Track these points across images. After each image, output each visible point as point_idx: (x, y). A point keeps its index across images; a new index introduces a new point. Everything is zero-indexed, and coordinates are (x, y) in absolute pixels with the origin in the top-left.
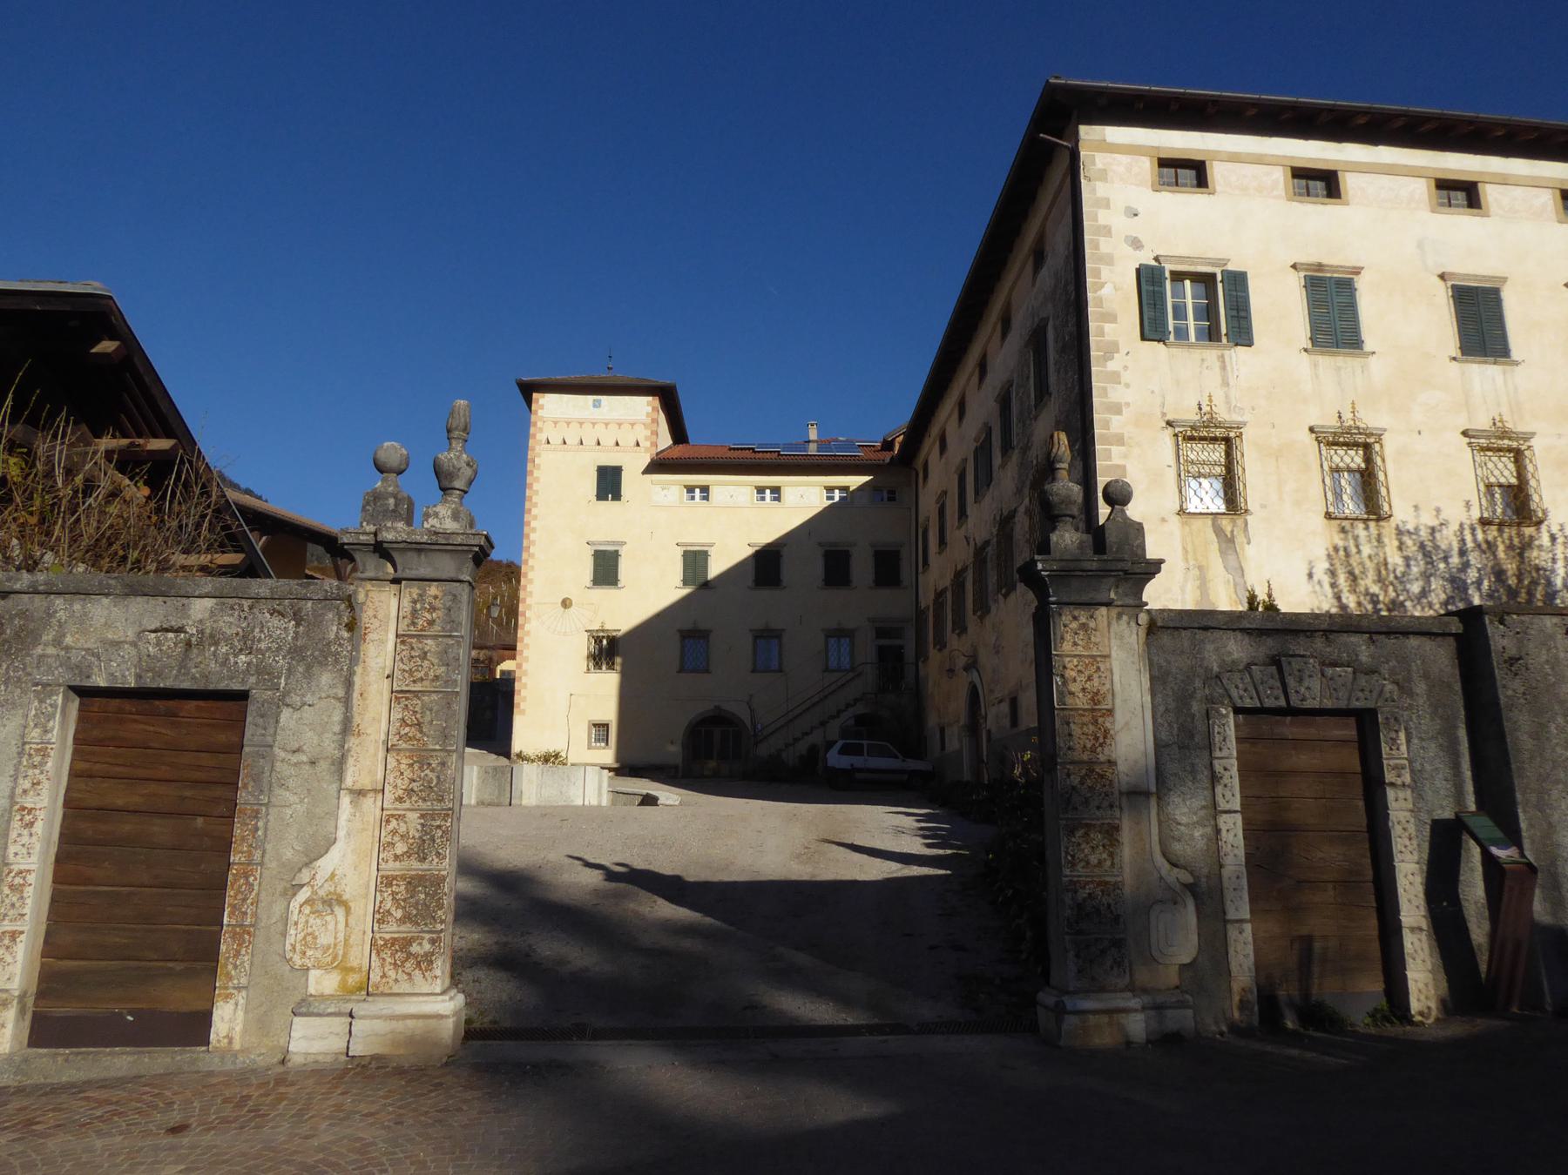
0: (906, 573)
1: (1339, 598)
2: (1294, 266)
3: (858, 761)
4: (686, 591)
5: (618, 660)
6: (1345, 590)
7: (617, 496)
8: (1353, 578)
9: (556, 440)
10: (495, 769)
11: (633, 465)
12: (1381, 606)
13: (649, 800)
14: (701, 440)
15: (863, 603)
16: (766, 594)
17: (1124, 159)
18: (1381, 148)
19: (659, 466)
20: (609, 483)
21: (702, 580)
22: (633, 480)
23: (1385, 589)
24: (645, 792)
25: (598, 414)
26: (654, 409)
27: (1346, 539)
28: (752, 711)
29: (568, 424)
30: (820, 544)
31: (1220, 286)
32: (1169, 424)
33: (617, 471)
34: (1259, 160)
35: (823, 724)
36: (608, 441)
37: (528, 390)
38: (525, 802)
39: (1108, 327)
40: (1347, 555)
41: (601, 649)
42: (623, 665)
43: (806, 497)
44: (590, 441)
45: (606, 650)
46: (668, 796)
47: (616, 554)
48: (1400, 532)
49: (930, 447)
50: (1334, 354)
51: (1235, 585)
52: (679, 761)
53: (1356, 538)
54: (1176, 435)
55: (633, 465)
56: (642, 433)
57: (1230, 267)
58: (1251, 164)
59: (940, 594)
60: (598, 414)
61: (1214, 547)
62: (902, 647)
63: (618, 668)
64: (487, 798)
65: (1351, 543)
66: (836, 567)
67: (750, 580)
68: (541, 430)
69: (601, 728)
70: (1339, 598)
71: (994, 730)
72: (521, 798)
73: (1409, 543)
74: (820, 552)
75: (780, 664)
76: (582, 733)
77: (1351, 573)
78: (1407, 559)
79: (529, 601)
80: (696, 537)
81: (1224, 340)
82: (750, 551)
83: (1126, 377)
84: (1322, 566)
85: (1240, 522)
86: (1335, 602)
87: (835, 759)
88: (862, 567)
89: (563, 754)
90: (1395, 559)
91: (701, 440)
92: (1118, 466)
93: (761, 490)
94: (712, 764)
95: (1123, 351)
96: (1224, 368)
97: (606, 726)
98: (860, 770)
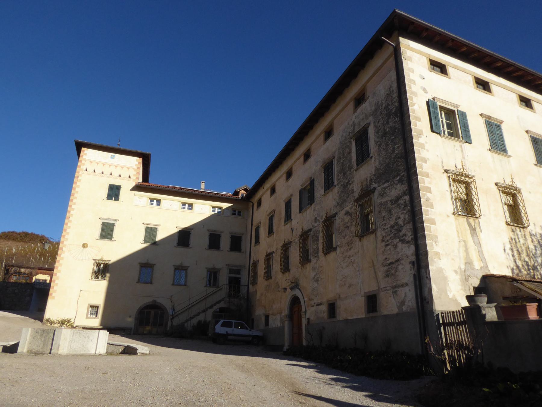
0: (245, 245)
1: (515, 262)
2: (481, 115)
3: (229, 330)
4: (146, 245)
5: (108, 275)
6: (517, 258)
7: (117, 199)
8: (519, 254)
9: (90, 170)
10: (43, 331)
11: (126, 186)
12: (530, 267)
13: (129, 351)
14: (152, 182)
15: (223, 259)
16: (182, 250)
17: (418, 56)
18: (501, 78)
19: (138, 188)
20: (114, 192)
21: (153, 241)
22: (125, 193)
23: (530, 259)
24: (126, 344)
25: (112, 161)
26: (139, 163)
27: (514, 235)
28: (172, 303)
29: (98, 163)
30: (208, 230)
31: (457, 116)
32: (446, 171)
33: (118, 188)
34: (464, 71)
35: (204, 311)
36: (116, 173)
37: (79, 146)
38: (60, 352)
39: (418, 123)
40: (516, 243)
41: (99, 269)
42: (110, 278)
43: (203, 210)
44: (107, 173)
45: (102, 270)
46: (142, 347)
47: (113, 225)
48: (531, 235)
49: (264, 193)
50: (499, 154)
51: (479, 251)
52: (132, 326)
53: (517, 235)
54: (449, 177)
55: (126, 186)
56: (132, 173)
57: (460, 109)
58: (462, 72)
59: (269, 256)
60: (112, 161)
61: (469, 232)
62: (240, 278)
63: (107, 279)
64: (35, 348)
65: (516, 237)
66: (214, 241)
67: (176, 242)
68: (84, 164)
69: (95, 308)
70: (515, 262)
71: (312, 318)
72: (58, 349)
73: (535, 240)
74: (209, 234)
75: (186, 282)
76: (84, 309)
77: (518, 251)
78: (535, 246)
79: (65, 243)
80: (152, 221)
81: (461, 138)
82: (177, 230)
83: (427, 146)
84: (508, 246)
85: (477, 221)
86: (514, 263)
87: (219, 329)
88: (225, 242)
89: (72, 321)
90: (532, 247)
91: (152, 182)
92: (428, 187)
93: (184, 204)
94: (148, 328)
95: (425, 135)
96: (462, 151)
97: (97, 307)
98: (231, 335)
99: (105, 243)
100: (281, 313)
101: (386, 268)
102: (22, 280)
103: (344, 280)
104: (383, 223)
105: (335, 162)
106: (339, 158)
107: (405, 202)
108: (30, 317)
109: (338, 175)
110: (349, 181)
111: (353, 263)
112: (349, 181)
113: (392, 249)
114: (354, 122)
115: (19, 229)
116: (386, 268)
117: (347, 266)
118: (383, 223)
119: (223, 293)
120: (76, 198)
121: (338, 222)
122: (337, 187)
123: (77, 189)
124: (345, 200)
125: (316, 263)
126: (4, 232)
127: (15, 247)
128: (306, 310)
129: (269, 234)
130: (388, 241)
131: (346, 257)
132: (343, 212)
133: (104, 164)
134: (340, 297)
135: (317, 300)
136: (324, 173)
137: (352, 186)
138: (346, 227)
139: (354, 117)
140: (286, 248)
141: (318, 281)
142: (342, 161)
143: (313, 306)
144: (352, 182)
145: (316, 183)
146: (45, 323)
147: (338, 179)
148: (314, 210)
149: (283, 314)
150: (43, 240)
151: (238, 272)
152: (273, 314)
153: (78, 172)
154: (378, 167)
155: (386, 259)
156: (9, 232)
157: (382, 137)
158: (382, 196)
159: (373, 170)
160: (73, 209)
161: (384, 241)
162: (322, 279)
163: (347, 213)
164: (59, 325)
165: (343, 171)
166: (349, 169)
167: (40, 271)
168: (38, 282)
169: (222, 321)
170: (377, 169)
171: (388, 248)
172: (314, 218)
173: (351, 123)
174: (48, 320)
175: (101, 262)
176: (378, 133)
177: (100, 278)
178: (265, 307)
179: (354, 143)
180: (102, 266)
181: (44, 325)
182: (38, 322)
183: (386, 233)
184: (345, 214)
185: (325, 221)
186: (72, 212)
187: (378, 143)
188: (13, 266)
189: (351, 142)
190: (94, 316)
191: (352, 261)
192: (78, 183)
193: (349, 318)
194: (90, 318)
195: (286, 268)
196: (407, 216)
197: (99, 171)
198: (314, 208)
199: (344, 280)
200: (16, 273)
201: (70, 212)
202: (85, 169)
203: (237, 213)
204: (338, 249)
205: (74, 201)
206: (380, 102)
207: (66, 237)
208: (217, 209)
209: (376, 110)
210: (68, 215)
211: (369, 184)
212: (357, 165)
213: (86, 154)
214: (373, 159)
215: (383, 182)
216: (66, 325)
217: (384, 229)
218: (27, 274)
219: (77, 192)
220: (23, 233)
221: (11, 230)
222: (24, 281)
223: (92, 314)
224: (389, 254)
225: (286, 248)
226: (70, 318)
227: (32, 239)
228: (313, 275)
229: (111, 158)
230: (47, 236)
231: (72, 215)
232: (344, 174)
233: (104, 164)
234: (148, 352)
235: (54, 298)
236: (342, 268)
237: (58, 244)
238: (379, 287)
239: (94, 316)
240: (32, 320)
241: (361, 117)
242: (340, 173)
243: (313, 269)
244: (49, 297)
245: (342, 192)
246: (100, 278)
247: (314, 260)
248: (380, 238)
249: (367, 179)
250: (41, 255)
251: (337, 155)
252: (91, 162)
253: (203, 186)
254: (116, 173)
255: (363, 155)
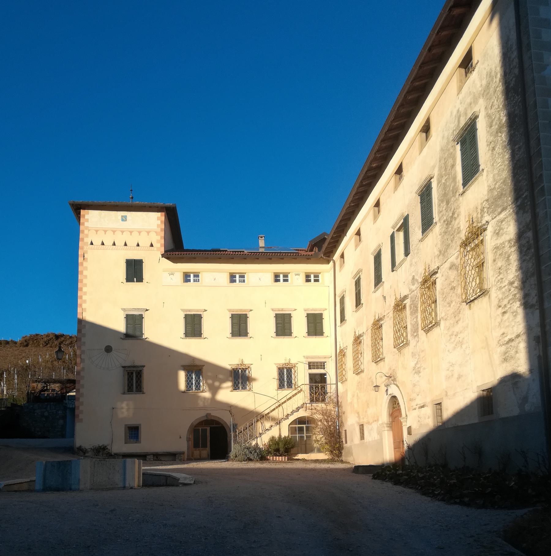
0: (328, 325)
7: (140, 279)
9: (97, 242)
20: (134, 270)
36: (132, 243)
37: (77, 209)
44: (120, 244)
62: (325, 374)
68: (87, 236)
71: (413, 427)
72: (352, 441)
88: (299, 325)
100: (378, 420)
101: (503, 348)
103: (451, 369)
104: (499, 278)
105: (434, 185)
106: (441, 176)
107: (528, 242)
109: (439, 205)
110: (453, 214)
111: (461, 343)
112: (453, 214)
113: (511, 318)
114: (458, 111)
116: (503, 348)
117: (454, 348)
118: (499, 278)
119: (303, 397)
121: (440, 280)
122: (438, 224)
124: (448, 246)
125: (416, 346)
128: (407, 416)
129: (357, 306)
130: (505, 306)
131: (452, 335)
132: (447, 265)
133: (114, 232)
134: (446, 395)
135: (419, 401)
136: (421, 203)
137: (457, 221)
138: (451, 289)
139: (458, 102)
140: (377, 325)
141: (419, 372)
142: (443, 181)
143: (415, 409)
144: (458, 215)
145: (411, 221)
147: (440, 212)
148: (411, 265)
149: (380, 422)
151: (322, 365)
152: (368, 423)
154: (493, 187)
155: (503, 334)
157: (497, 132)
158: (498, 234)
159: (486, 193)
160: (85, 301)
161: (500, 306)
162: (424, 369)
163: (452, 267)
165: (446, 199)
166: (453, 193)
170: (491, 190)
171: (506, 316)
172: (411, 278)
173: (455, 112)
176: (491, 127)
178: (358, 413)
179: (458, 147)
183: (504, 293)
184: (450, 268)
185: (425, 281)
187: (492, 145)
189: (455, 149)
191: (461, 339)
193: (460, 424)
195: (377, 359)
196: (530, 265)
198: (411, 261)
199: (451, 369)
204: (442, 323)
205: (85, 289)
206: (494, 69)
209: (488, 86)
211: (479, 216)
212: (464, 185)
214: (485, 173)
215: (499, 210)
217: (501, 288)
223: (131, 437)
224: (508, 326)
225: (377, 325)
228: (412, 364)
231: (85, 309)
232: (448, 203)
233: (114, 232)
234: (192, 482)
236: (449, 351)
238: (82, 451)
241: (468, 100)
242: (442, 201)
243: (413, 354)
245: (445, 233)
247: (412, 342)
248: (495, 302)
249: (477, 208)
251: (436, 173)
253: (262, 243)
254: (132, 243)
255: (471, 169)
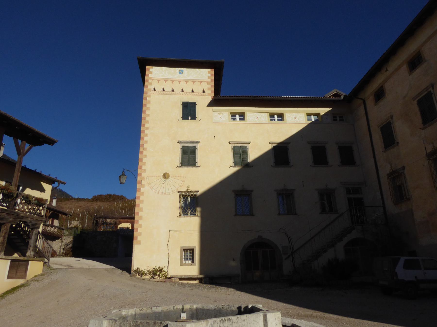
4: (236, 169)
5: (199, 209)
7: (194, 117)
9: (159, 89)
11: (203, 100)
20: (189, 111)
22: (202, 110)
25: (181, 77)
29: (166, 81)
33: (193, 105)
36: (188, 89)
37: (143, 64)
42: (202, 212)
43: (296, 120)
44: (178, 89)
45: (191, 203)
47: (194, 149)
60: (181, 77)
63: (199, 214)
66: (319, 155)
68: (151, 84)
69: (188, 253)
76: (177, 255)
82: (270, 147)
88: (333, 156)
89: (165, 269)
94: (257, 273)
99: (188, 170)
102: (109, 229)
108: (117, 267)
115: (104, 193)
120: (148, 122)
123: (147, 112)
126: (95, 196)
127: (104, 206)
133: (173, 81)
146: (133, 275)
150: (122, 198)
153: (147, 93)
156: (98, 196)
160: (147, 135)
164: (150, 276)
167: (122, 220)
168: (122, 229)
169: (402, 260)
174: (137, 271)
175: (188, 194)
177: (189, 214)
180: (189, 199)
181: (133, 278)
182: (126, 274)
186: (146, 139)
188: (100, 218)
190: (190, 262)
192: (148, 105)
194: (186, 265)
197: (168, 89)
200: (103, 223)
201: (143, 139)
202: (152, 89)
203: (338, 119)
205: (147, 125)
207: (144, 167)
208: (312, 116)
210: (141, 142)
213: (151, 73)
216: (159, 275)
218: (112, 224)
219: (147, 129)
220: (108, 195)
221: (99, 194)
222: (111, 230)
223: (186, 259)
226: (162, 266)
227: (115, 199)
229: (180, 73)
230: (124, 196)
235: (139, 243)
237: (134, 201)
239: (190, 262)
240: (119, 271)
244: (135, 241)
246: (189, 214)
250: (122, 209)
252: (159, 81)
254: (188, 89)
